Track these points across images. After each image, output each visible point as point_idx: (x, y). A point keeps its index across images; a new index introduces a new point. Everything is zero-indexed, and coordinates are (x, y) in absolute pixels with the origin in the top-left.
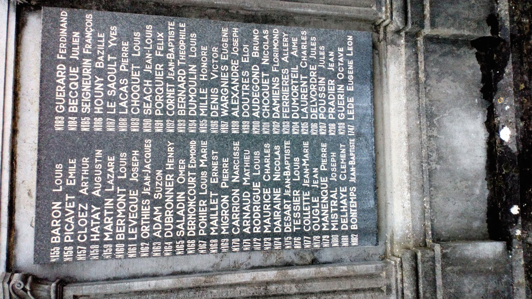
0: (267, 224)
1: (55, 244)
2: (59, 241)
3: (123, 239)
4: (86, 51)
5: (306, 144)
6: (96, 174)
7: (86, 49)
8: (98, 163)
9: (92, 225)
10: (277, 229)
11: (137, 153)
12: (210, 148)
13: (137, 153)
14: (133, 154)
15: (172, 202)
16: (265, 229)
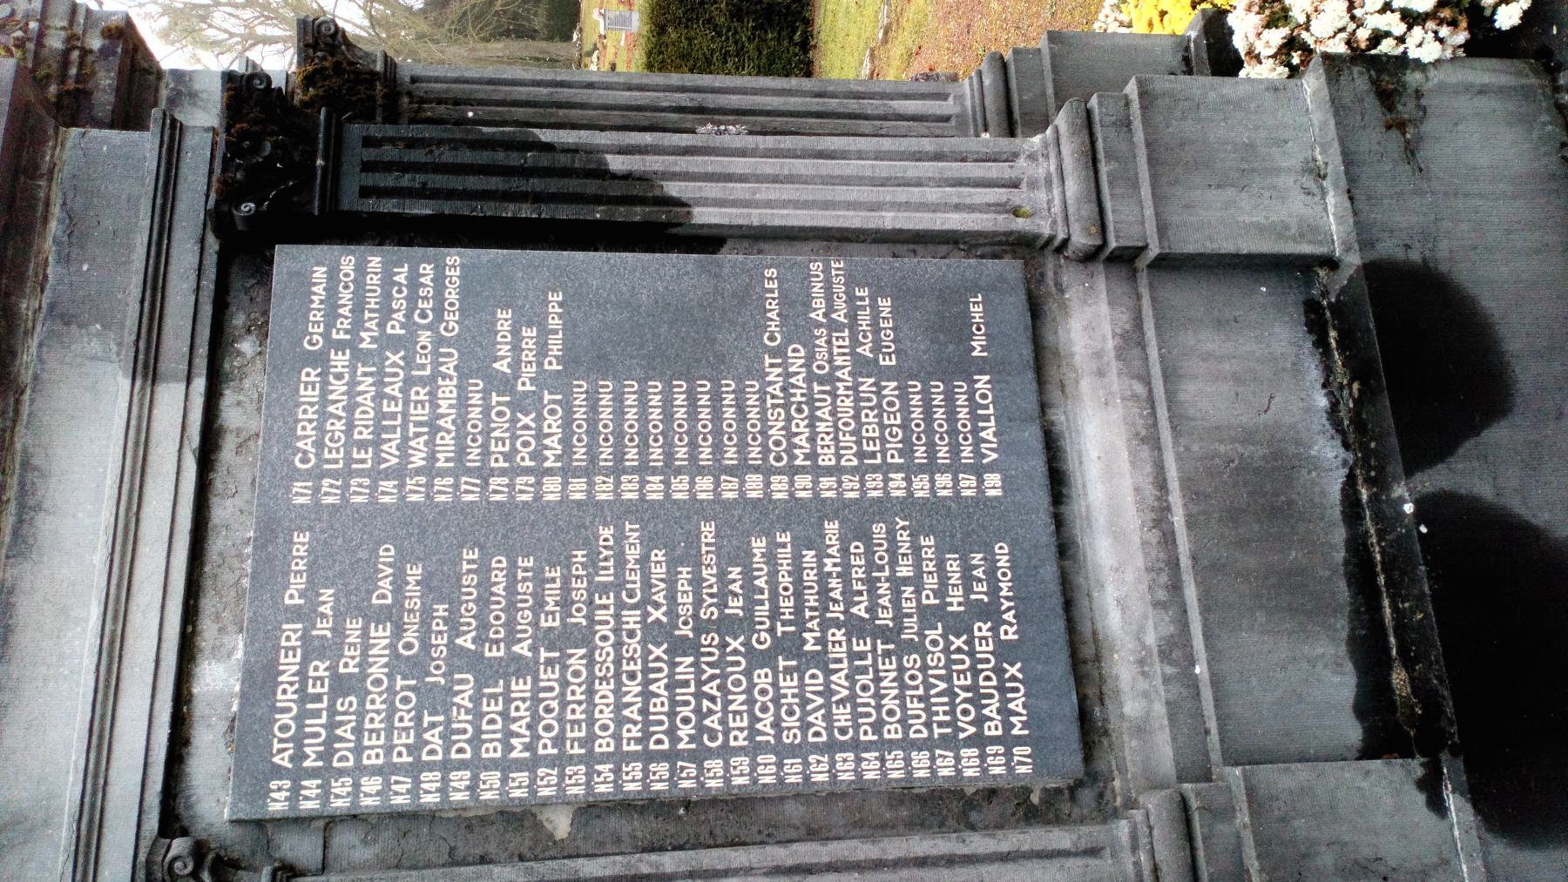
0: (1019, 714)
1: (891, 741)
2: (611, 749)
3: (499, 755)
4: (338, 333)
5: (708, 531)
6: (519, 605)
7: (338, 331)
8: (525, 580)
9: (425, 725)
10: (432, 752)
11: (583, 556)
12: (649, 543)
13: (583, 556)
14: (575, 560)
15: (386, 674)
16: (513, 748)
